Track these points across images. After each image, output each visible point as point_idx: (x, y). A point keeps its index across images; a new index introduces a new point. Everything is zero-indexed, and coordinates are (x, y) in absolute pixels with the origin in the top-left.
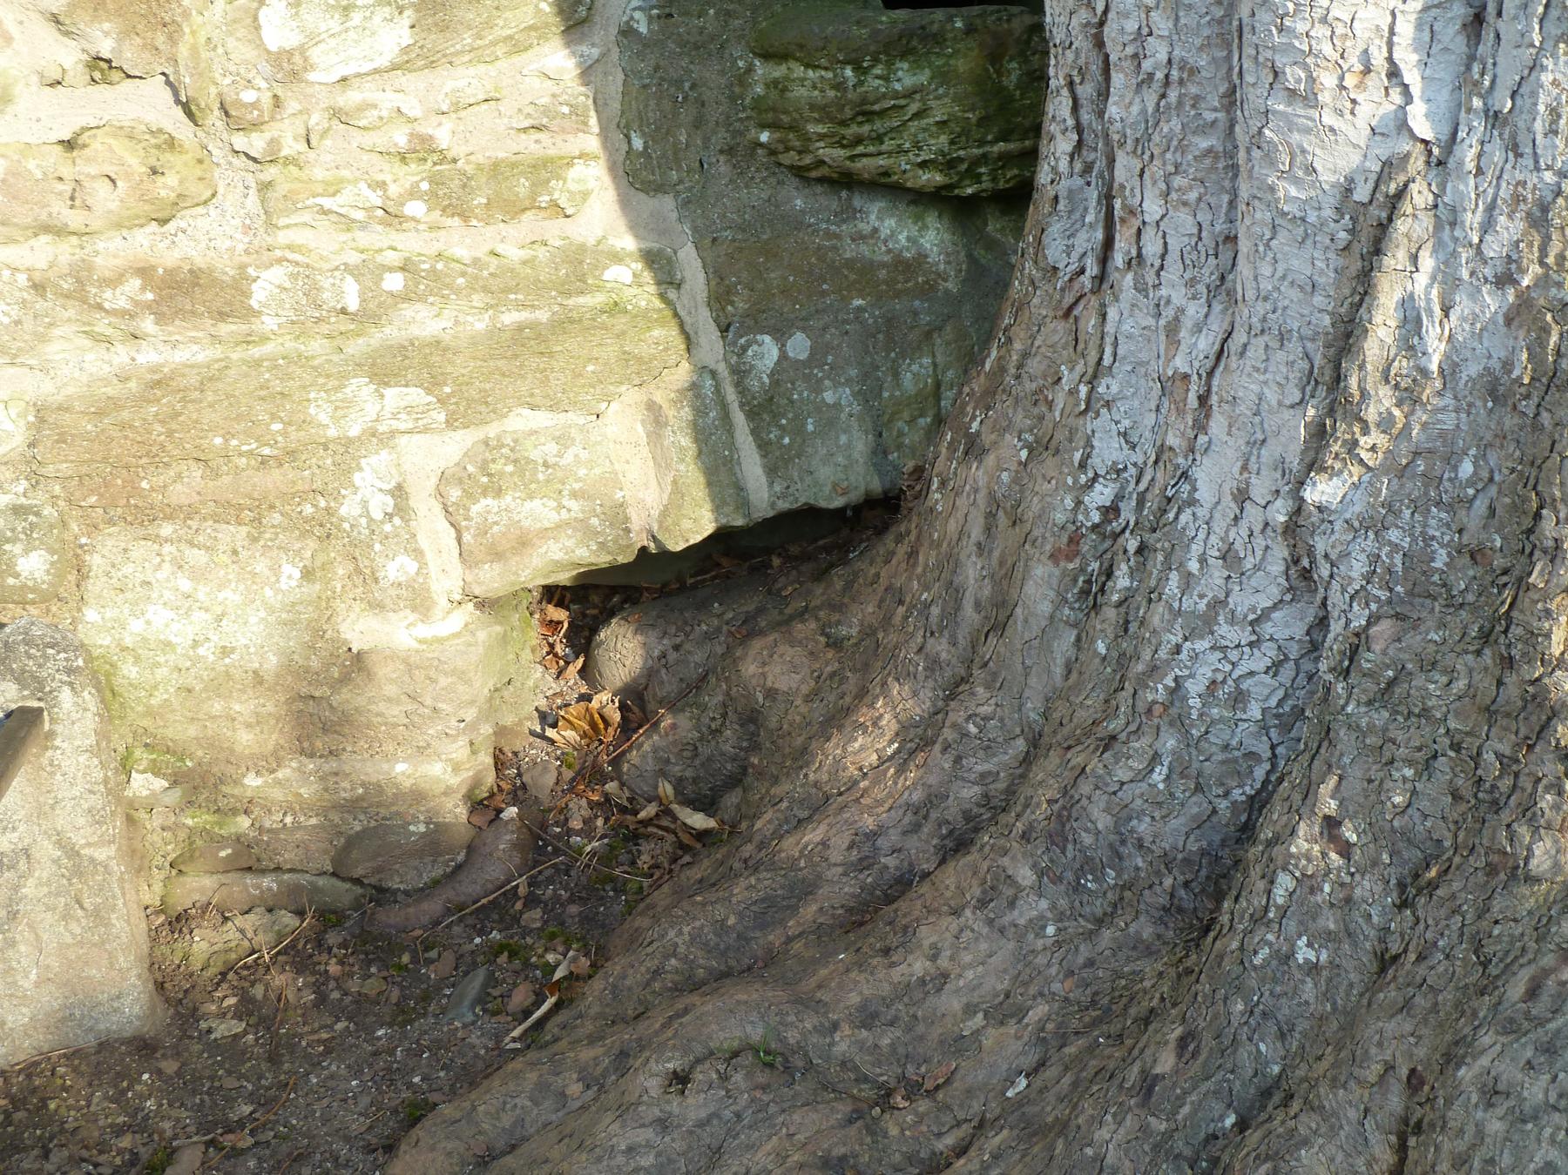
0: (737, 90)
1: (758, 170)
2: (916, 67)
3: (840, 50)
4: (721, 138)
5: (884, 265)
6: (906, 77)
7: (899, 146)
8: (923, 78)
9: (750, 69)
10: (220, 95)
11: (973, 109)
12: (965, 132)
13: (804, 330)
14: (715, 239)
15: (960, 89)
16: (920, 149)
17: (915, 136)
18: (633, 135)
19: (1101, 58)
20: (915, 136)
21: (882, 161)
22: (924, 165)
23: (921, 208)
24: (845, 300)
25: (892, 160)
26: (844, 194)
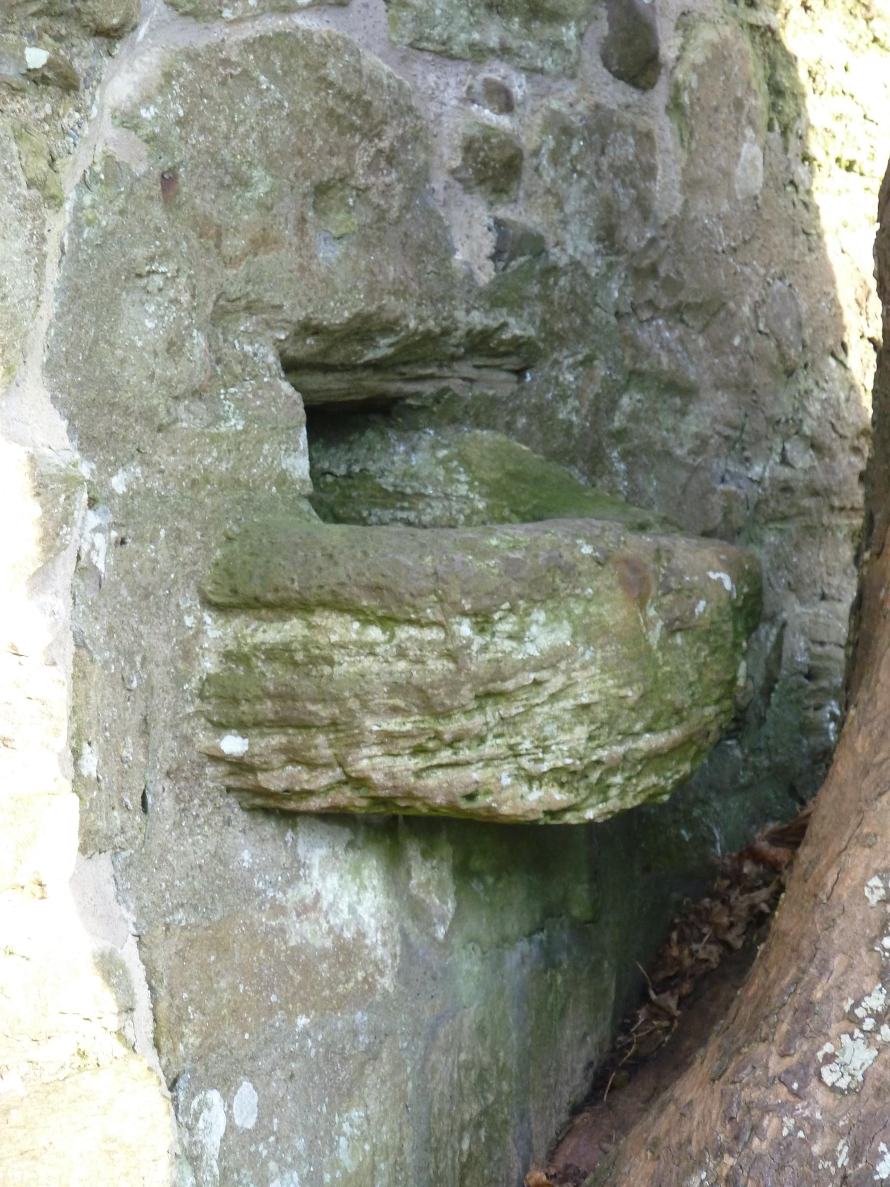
0: (180, 665)
1: (203, 804)
2: (554, 618)
3: (466, 594)
4: (167, 749)
5: (324, 954)
6: (545, 634)
7: (511, 747)
8: (563, 635)
9: (199, 631)
10: (547, 681)
11: (629, 684)
12: (610, 723)
13: (252, 1076)
14: (168, 927)
15: (610, 650)
16: (546, 750)
17: (541, 728)
18: (86, 749)
19: (311, 596)
20: (541, 728)
21: (475, 774)
22: (531, 779)
23: (358, 855)
24: (291, 1016)
25: (490, 771)
26: (289, 836)
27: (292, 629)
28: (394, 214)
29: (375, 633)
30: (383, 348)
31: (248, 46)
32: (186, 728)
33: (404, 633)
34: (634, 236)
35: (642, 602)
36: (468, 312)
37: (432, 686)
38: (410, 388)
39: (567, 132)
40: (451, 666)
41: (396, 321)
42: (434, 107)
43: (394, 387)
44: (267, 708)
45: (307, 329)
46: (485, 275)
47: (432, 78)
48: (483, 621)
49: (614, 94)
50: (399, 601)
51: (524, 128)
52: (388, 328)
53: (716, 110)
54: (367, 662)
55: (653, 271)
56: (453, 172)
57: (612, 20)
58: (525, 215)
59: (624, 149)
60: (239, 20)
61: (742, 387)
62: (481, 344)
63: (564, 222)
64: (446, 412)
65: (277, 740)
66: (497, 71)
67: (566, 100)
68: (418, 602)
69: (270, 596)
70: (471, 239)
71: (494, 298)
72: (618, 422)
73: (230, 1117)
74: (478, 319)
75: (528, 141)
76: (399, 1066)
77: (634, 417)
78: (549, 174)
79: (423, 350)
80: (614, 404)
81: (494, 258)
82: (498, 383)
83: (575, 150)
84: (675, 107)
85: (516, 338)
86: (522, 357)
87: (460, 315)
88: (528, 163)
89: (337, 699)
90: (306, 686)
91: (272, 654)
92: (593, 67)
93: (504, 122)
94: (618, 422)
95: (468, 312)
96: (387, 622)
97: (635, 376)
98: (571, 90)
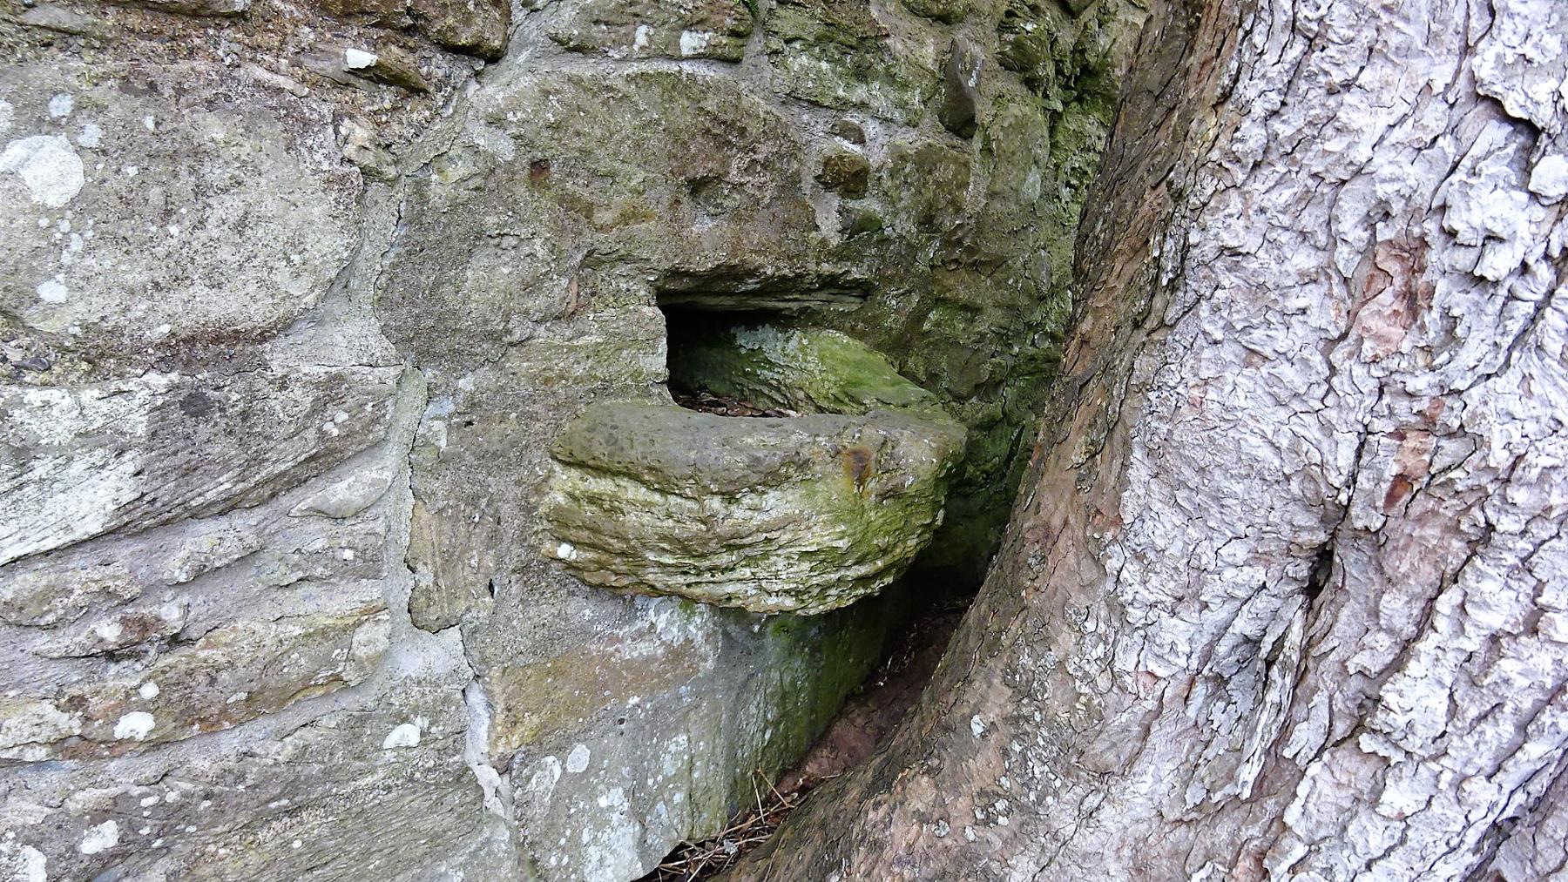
21: (730, 588)
27: (603, 486)
28: (766, 200)
29: (657, 497)
30: (751, 284)
31: (630, 79)
32: (533, 540)
33: (672, 499)
34: (948, 222)
35: (861, 481)
36: (818, 264)
37: (687, 539)
38: (781, 305)
39: (903, 158)
40: (703, 527)
41: (756, 269)
42: (806, 137)
43: (771, 304)
44: (584, 535)
45: (675, 273)
46: (835, 241)
47: (805, 117)
48: (730, 498)
49: (942, 140)
50: (668, 482)
51: (876, 154)
52: (751, 273)
53: (1013, 153)
54: (646, 518)
55: (959, 242)
56: (817, 178)
57: (948, 95)
58: (870, 205)
59: (945, 173)
60: (624, 59)
61: (1011, 308)
62: (830, 283)
63: (896, 214)
64: (810, 320)
65: (591, 555)
66: (853, 118)
67: (908, 140)
68: (681, 484)
69: (591, 462)
70: (829, 226)
71: (839, 255)
72: (926, 327)
73: (564, 769)
74: (826, 268)
75: (874, 162)
76: (715, 708)
77: (938, 324)
78: (887, 183)
79: (779, 286)
80: (925, 316)
81: (842, 232)
82: (850, 304)
83: (907, 170)
84: (987, 150)
85: (856, 280)
86: (864, 290)
87: (812, 266)
88: (873, 176)
89: (627, 540)
90: (607, 526)
91: (593, 500)
92: (929, 120)
93: (857, 149)
94: (926, 327)
95: (818, 264)
96: (662, 492)
97: (939, 302)
98: (913, 134)
